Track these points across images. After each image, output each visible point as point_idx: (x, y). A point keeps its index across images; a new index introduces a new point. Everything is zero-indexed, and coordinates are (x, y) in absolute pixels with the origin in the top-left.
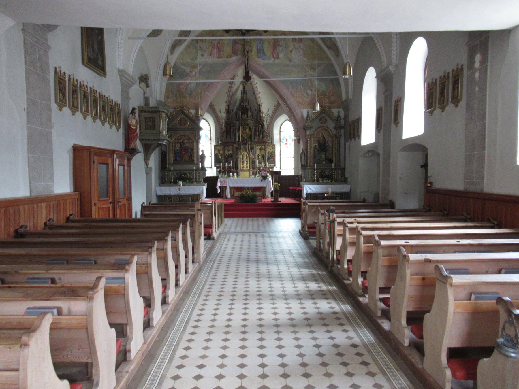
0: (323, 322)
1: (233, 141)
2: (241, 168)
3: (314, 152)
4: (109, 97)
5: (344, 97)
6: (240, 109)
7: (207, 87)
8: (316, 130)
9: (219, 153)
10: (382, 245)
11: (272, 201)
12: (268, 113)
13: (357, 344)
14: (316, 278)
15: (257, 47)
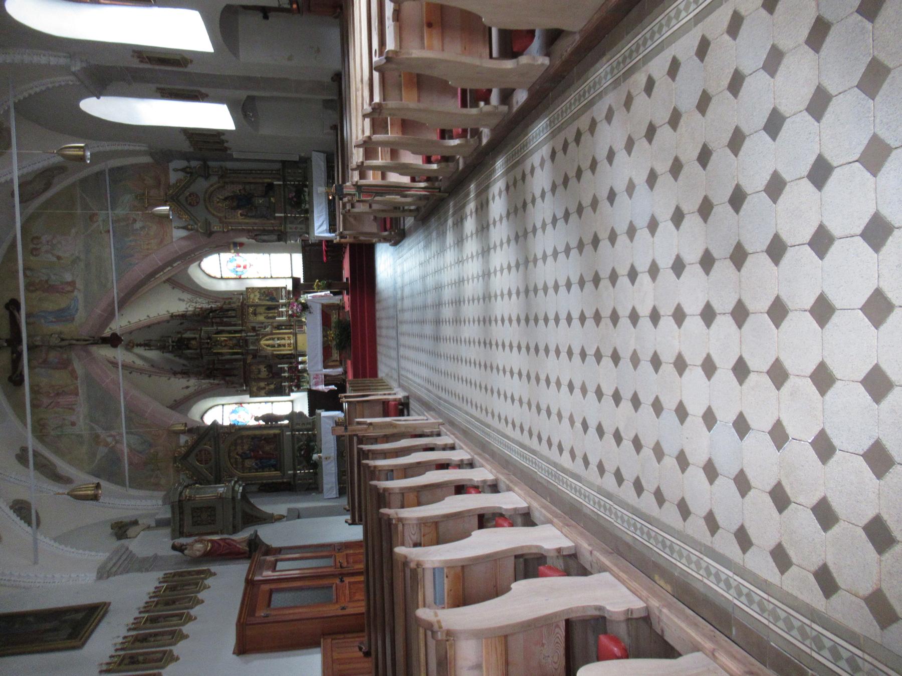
0: (520, 211)
1: (242, 363)
3: (252, 217)
4: (149, 594)
5: (146, 159)
6: (180, 352)
7: (134, 414)
9: (264, 388)
10: (380, 100)
11: (348, 294)
12: (186, 300)
13: (550, 151)
14: (459, 220)
15: (52, 322)
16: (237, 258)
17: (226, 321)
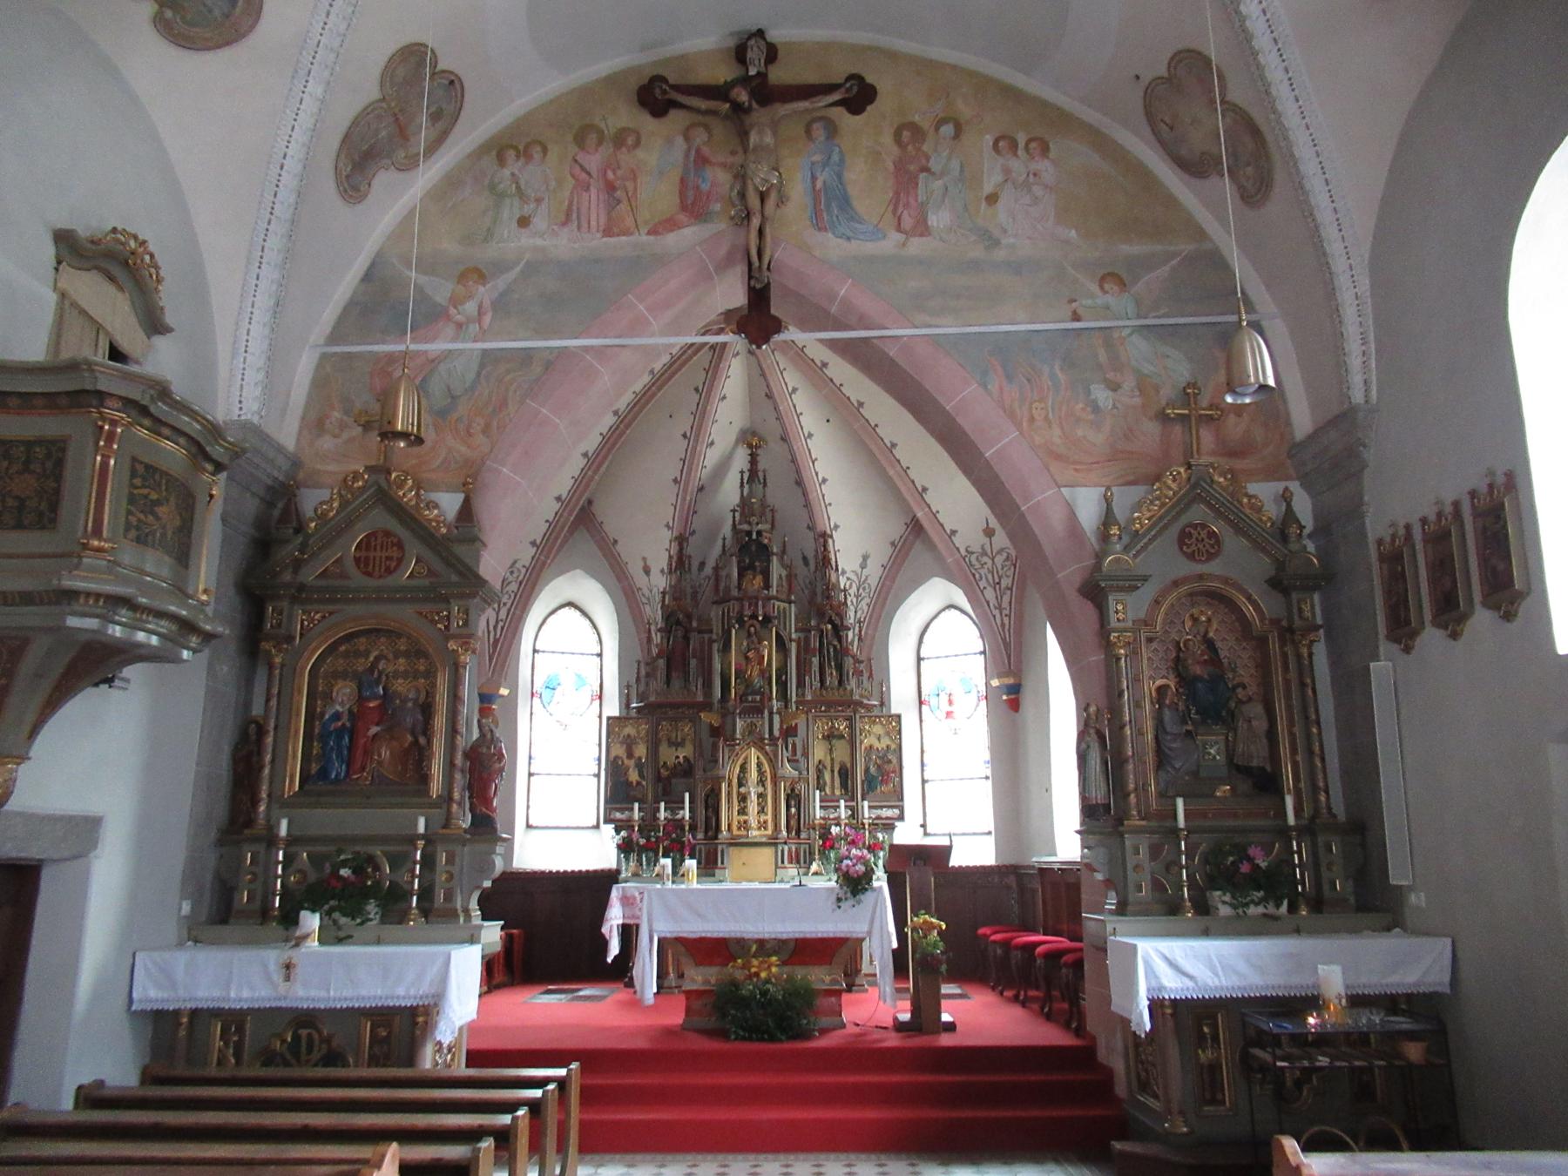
1: (700, 698)
2: (735, 832)
8: (1164, 593)
9: (630, 755)
11: (899, 1027)
15: (814, 178)
16: (973, 697)
17: (811, 663)
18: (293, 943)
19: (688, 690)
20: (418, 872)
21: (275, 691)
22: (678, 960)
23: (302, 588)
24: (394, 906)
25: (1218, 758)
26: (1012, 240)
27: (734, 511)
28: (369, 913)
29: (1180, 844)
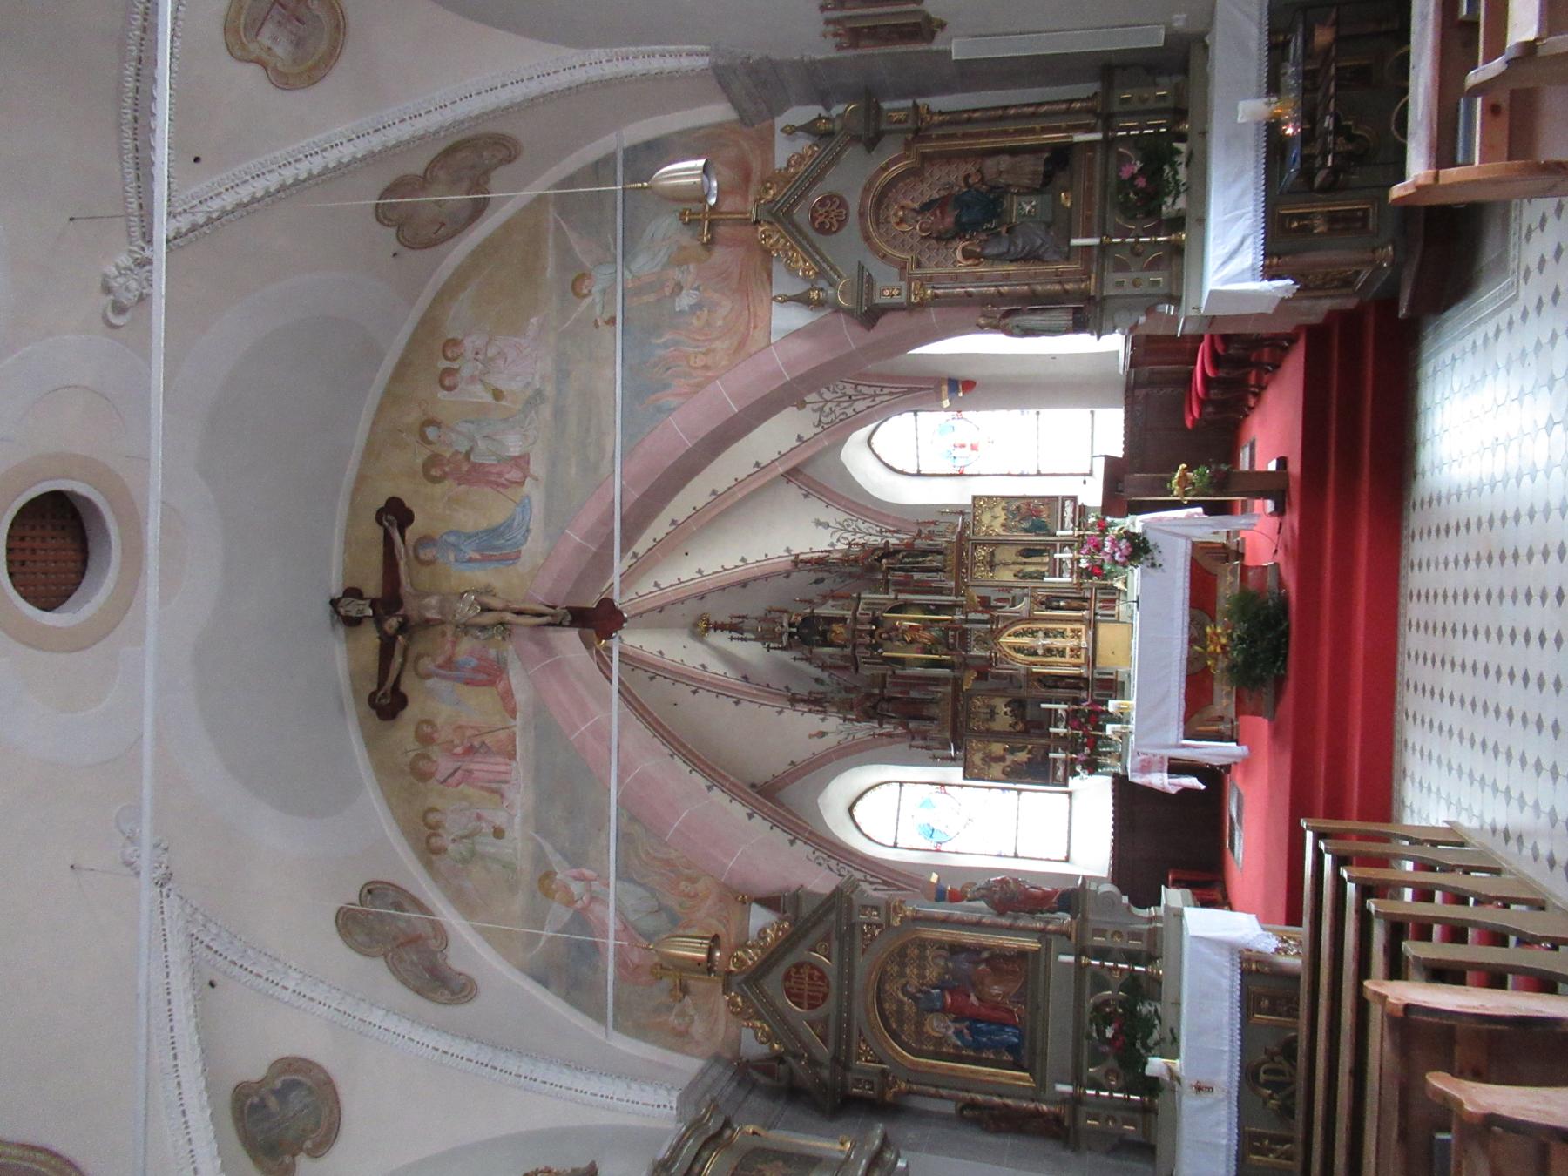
1: (949, 689)
3: (999, 258)
8: (875, 250)
9: (1001, 759)
11: (1280, 511)
15: (470, 560)
18: (1176, 1083)
19: (941, 700)
20: (1112, 964)
21: (932, 1090)
22: (1208, 720)
23: (835, 1059)
24: (1143, 989)
25: (1034, 203)
26: (537, 377)
27: (769, 648)
28: (1150, 1012)
29: (1116, 243)
